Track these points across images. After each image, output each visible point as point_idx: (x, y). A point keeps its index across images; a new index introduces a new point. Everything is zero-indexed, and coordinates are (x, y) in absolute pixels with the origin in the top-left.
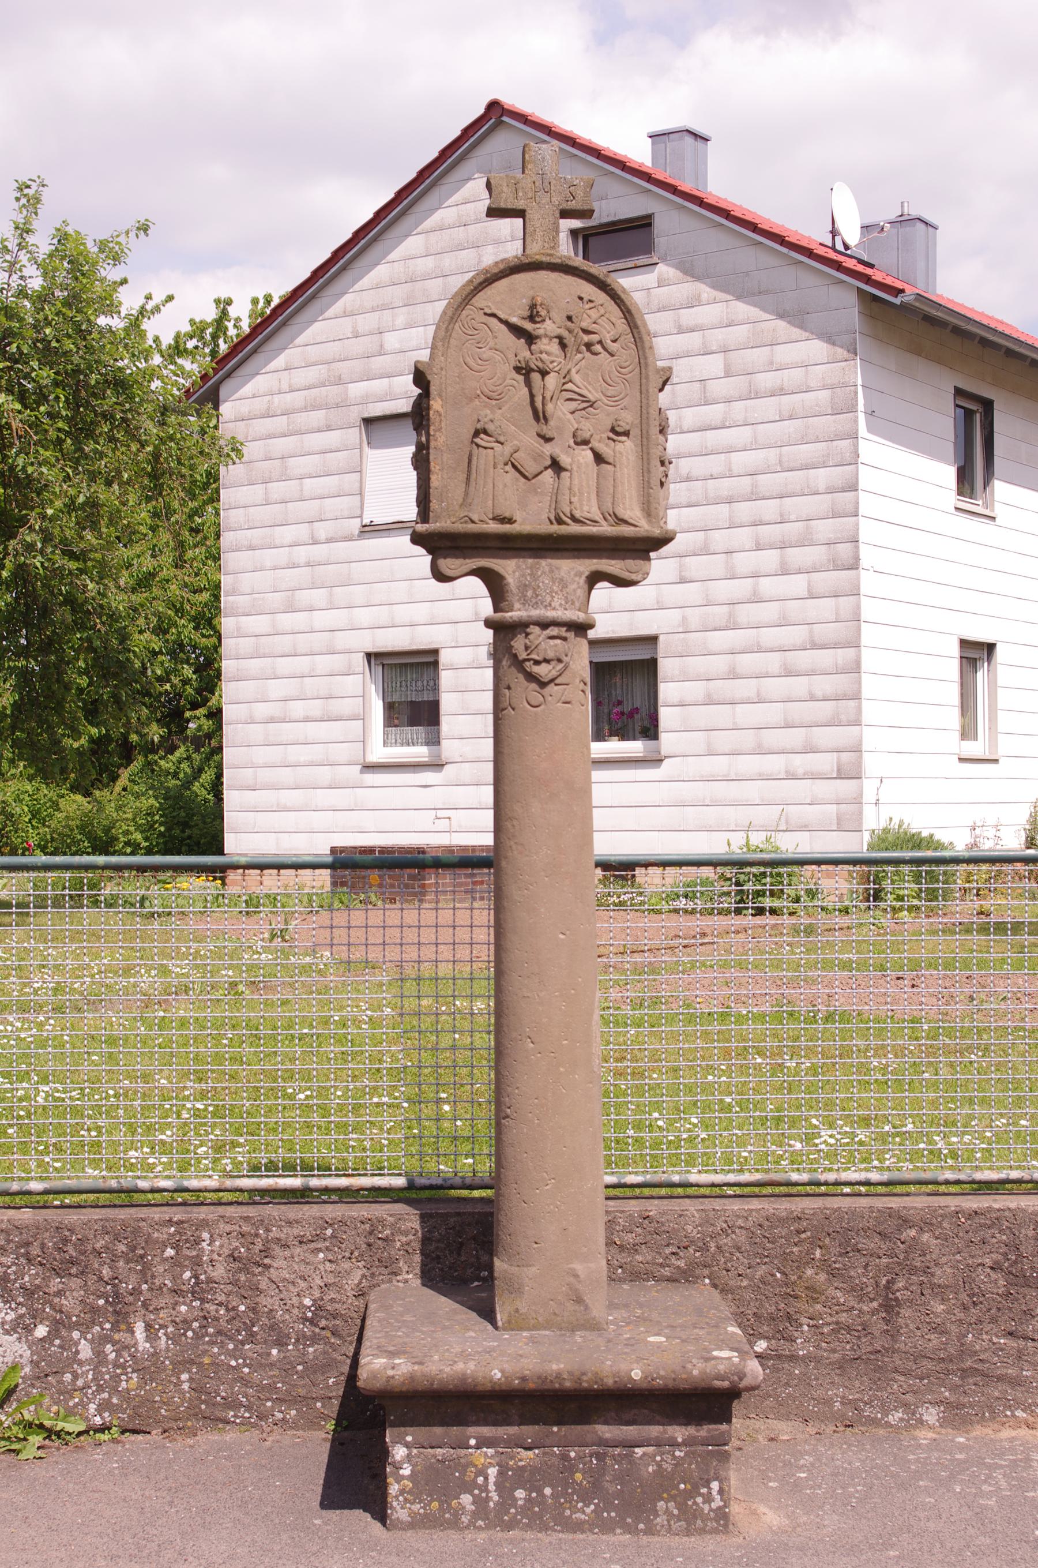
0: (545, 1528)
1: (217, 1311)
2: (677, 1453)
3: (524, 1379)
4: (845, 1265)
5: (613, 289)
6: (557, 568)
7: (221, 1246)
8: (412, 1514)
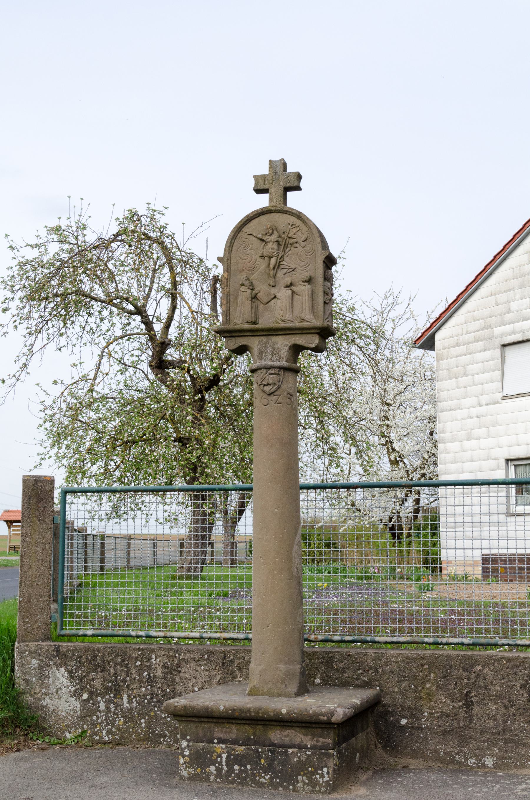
0: (247, 784)
1: (158, 691)
2: (308, 753)
3: (233, 711)
4: (445, 683)
7: (160, 661)
8: (189, 773)
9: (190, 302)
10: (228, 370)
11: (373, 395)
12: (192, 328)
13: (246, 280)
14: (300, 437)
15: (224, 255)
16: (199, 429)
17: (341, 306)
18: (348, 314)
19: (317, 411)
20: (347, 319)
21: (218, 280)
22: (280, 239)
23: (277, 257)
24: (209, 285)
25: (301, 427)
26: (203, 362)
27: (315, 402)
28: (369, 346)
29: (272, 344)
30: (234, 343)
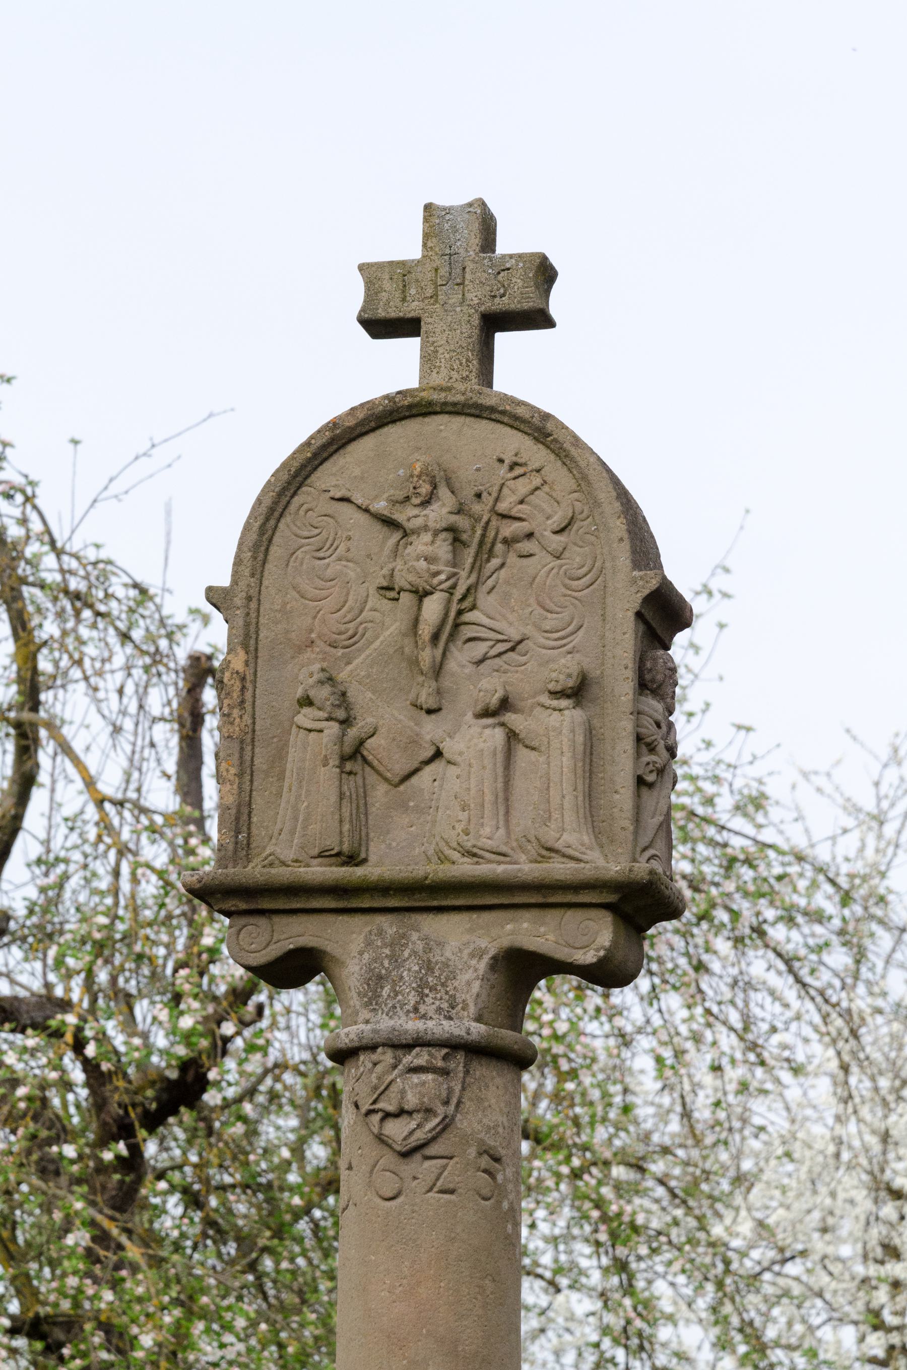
5: (555, 441)
6: (439, 944)
9: (92, 763)
10: (239, 1042)
11: (837, 1155)
12: (101, 869)
13: (321, 682)
14: (529, 1323)
15: (235, 581)
16: (115, 1285)
17: (708, 787)
18: (738, 823)
19: (605, 1218)
20: (737, 842)
21: (211, 671)
22: (462, 522)
23: (451, 591)
24: (172, 691)
25: (539, 1284)
26: (141, 1009)
27: (600, 1183)
28: (826, 958)
29: (420, 946)
30: (267, 937)
